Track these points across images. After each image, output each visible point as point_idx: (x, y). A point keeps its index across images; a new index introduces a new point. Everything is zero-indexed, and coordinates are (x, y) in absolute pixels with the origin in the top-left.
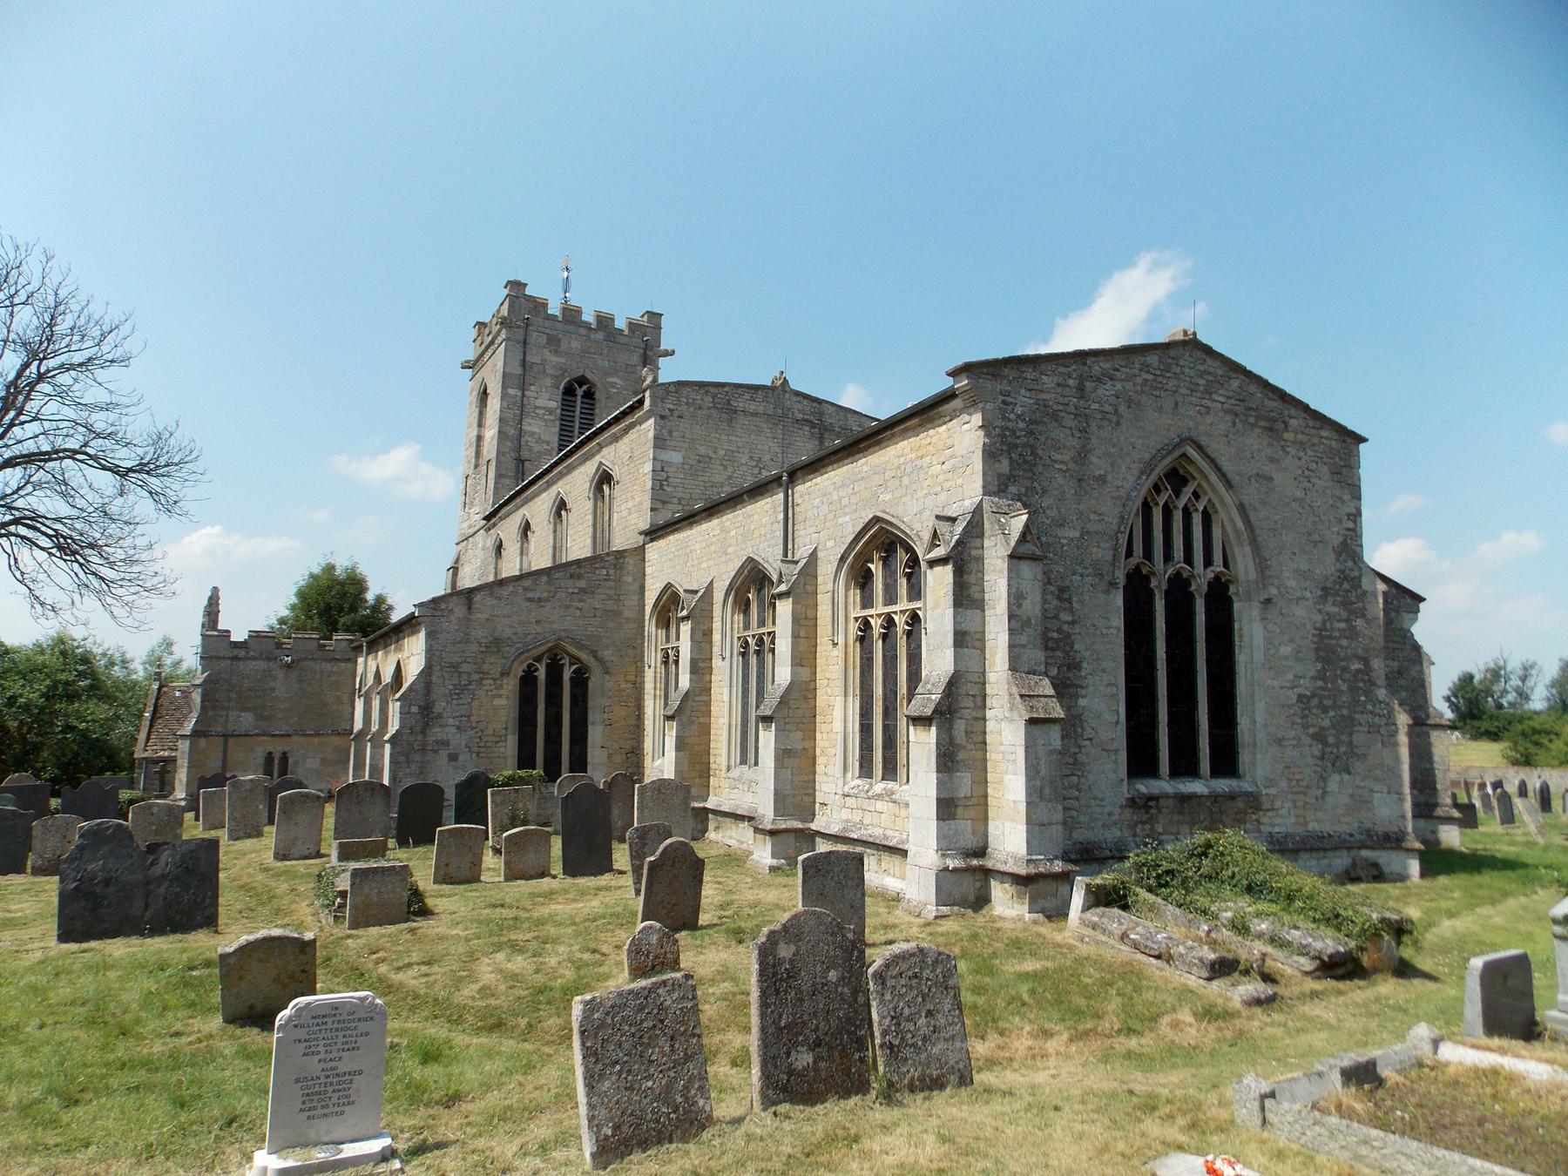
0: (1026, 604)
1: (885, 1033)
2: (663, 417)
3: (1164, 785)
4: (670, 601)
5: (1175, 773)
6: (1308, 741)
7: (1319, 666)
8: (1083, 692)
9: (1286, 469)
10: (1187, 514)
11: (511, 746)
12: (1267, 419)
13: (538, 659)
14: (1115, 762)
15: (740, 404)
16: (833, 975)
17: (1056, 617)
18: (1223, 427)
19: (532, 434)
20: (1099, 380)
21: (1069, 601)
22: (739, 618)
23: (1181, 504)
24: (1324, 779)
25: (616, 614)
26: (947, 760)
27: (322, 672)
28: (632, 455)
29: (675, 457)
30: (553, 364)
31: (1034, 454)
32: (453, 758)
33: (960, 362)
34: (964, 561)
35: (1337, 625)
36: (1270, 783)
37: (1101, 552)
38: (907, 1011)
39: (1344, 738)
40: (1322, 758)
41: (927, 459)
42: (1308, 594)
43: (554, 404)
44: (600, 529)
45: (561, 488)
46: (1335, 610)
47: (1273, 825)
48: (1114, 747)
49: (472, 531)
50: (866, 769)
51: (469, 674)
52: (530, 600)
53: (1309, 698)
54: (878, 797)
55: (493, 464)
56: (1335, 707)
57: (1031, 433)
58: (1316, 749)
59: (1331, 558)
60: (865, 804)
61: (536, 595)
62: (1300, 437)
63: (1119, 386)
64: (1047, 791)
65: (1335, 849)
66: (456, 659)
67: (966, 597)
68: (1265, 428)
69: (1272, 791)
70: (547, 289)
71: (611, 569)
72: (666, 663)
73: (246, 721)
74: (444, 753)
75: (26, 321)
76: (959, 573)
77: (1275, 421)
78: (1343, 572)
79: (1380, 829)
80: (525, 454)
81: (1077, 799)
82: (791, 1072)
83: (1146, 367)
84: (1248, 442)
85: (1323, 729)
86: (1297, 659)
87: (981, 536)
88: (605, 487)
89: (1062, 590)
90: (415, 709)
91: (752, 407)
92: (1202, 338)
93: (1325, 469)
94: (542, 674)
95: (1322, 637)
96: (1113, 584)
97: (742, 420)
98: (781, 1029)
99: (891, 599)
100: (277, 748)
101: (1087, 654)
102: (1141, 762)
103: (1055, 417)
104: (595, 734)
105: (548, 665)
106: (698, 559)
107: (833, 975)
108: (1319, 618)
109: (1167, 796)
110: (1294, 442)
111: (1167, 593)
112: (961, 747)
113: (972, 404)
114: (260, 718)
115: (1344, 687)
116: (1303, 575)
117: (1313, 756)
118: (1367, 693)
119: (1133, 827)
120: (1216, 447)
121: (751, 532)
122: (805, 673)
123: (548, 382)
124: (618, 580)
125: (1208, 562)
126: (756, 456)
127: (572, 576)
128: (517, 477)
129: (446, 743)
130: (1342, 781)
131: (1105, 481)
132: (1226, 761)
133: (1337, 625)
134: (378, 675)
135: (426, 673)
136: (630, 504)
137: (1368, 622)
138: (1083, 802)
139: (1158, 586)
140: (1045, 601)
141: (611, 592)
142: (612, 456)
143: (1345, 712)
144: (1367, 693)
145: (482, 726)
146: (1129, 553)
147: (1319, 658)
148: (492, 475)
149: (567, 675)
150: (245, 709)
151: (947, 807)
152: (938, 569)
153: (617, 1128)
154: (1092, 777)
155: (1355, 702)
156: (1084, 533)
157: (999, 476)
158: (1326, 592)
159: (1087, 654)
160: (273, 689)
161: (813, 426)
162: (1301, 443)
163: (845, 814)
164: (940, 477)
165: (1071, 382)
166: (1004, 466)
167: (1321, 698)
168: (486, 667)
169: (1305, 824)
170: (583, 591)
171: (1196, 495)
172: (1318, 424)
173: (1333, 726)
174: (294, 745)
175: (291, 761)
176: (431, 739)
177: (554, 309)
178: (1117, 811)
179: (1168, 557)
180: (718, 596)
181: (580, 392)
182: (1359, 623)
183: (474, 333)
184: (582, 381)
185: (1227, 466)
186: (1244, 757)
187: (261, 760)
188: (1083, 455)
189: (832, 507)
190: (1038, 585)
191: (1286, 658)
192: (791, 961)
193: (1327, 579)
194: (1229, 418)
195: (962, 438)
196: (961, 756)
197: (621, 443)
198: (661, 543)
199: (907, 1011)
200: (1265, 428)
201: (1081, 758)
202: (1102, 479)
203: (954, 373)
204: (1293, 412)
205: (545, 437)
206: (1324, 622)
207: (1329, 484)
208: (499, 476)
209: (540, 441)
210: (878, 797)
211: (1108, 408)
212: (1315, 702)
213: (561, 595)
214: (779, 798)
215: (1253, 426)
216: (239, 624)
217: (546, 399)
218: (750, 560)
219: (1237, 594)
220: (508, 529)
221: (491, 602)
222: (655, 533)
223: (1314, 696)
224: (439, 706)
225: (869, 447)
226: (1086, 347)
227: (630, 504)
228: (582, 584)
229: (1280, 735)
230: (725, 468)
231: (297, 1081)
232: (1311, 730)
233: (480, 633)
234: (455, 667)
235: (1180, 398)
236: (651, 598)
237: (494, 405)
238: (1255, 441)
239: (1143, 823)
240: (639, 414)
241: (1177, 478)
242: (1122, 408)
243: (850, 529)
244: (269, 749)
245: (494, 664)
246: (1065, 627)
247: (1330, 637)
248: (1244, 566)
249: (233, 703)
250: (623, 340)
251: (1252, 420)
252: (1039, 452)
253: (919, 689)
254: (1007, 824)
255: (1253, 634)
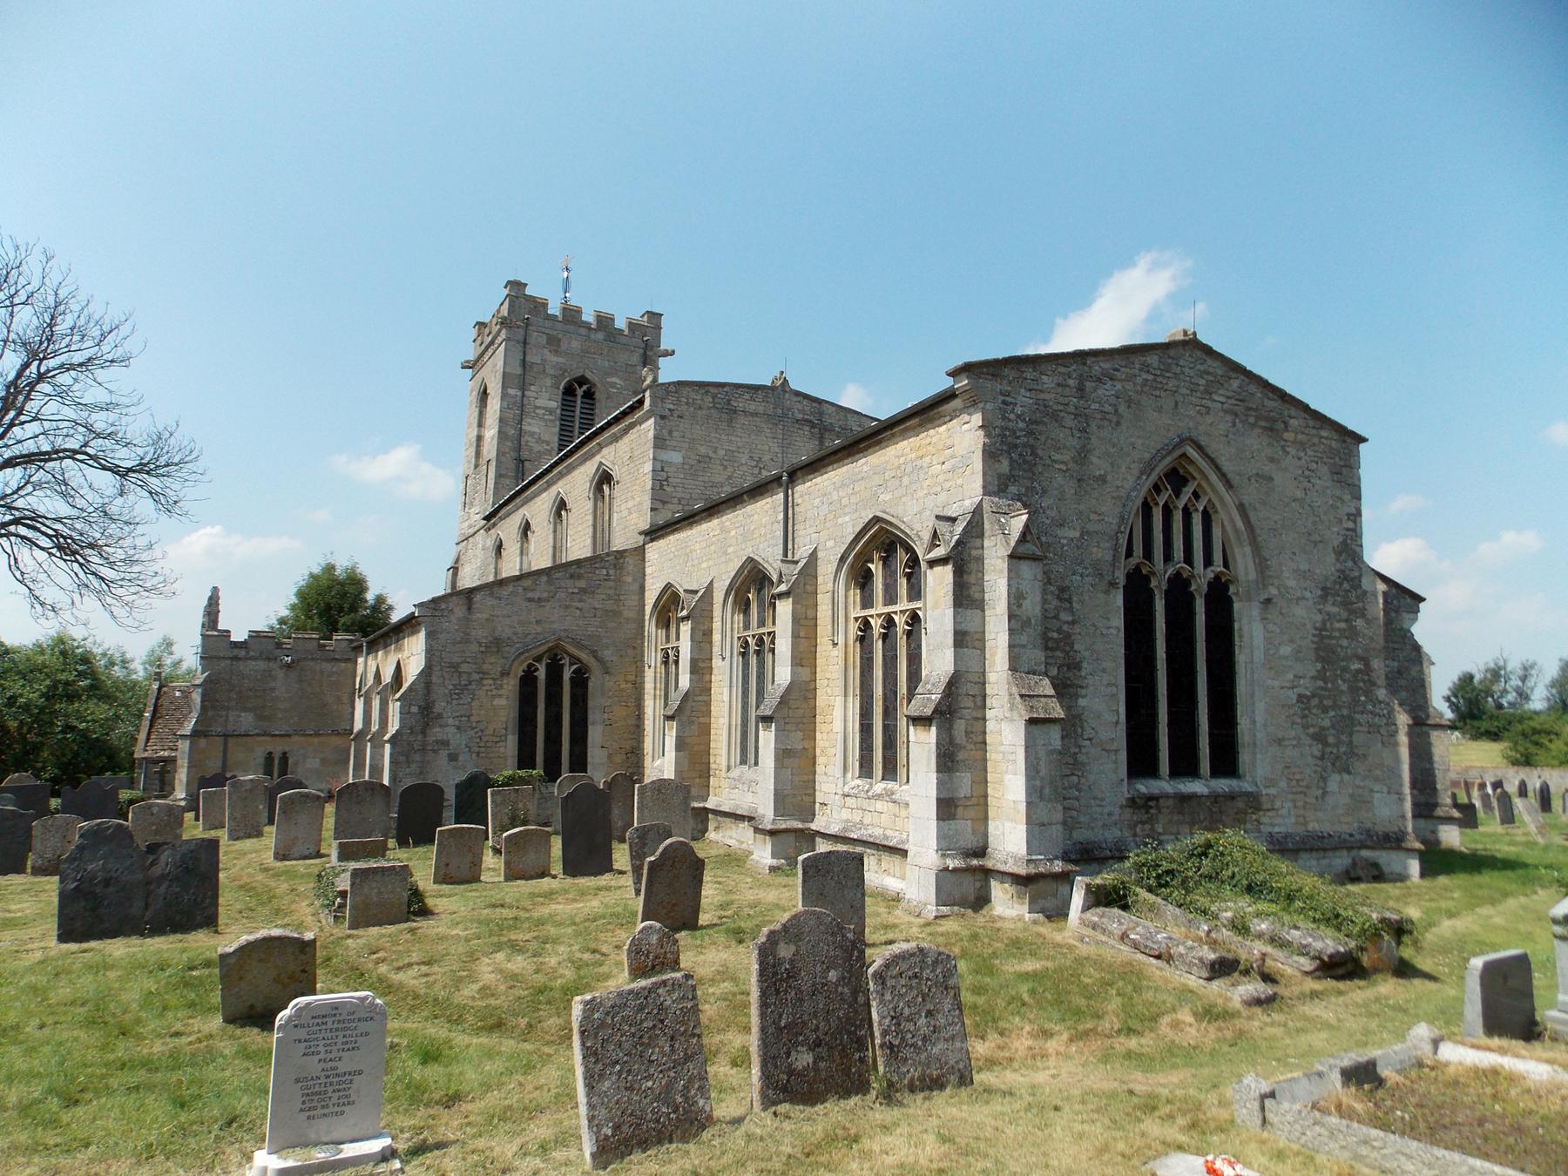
0: (1026, 604)
1: (885, 1033)
2: (663, 417)
3: (1164, 785)
4: (670, 601)
5: (1175, 773)
6: (1308, 741)
7: (1319, 666)
8: (1083, 692)
9: (1286, 469)
10: (1187, 514)
11: (511, 746)
12: (1267, 419)
13: (538, 659)
14: (1115, 762)
15: (740, 404)
16: (833, 975)
17: (1056, 617)
18: (1223, 427)
19: (532, 434)
20: (1099, 380)
21: (1069, 601)
22: (739, 618)
23: (1181, 504)
24: (1324, 779)
25: (616, 614)
26: (947, 760)
27: (322, 672)
28: (632, 455)
29: (675, 457)
30: (553, 364)
31: (1034, 454)
32: (453, 758)
33: (960, 362)
34: (964, 561)
35: (1337, 625)
36: (1270, 783)
37: (1101, 552)
38: (907, 1011)
39: (1344, 738)
40: (1322, 758)
41: (927, 459)
42: (1308, 594)
43: (554, 404)
44: (600, 529)
45: (561, 488)
46: (1335, 610)
47: (1273, 825)
48: (1114, 747)
49: (472, 531)
50: (866, 769)
51: (469, 674)
52: (530, 600)
53: (1309, 698)
54: (878, 797)
55: (493, 464)
56: (1335, 707)
57: (1031, 433)
58: (1316, 749)
59: (1331, 558)
60: (865, 804)
61: (536, 595)
62: (1300, 437)
63: (1119, 386)
64: (1047, 791)
65: (1335, 849)
66: (456, 659)
67: (966, 597)
68: (1265, 428)
69: (1272, 791)
70: (547, 289)
71: (611, 569)
72: (666, 663)
73: (246, 721)
74: (444, 753)
75: (26, 321)
76: (959, 573)
77: (1275, 421)
78: (1343, 572)
79: (1380, 829)
80: (525, 454)
81: (1077, 799)
82: (791, 1072)
83: (1146, 367)
84: (1248, 442)
85: (1323, 729)
86: (1297, 659)
87: (981, 536)
88: (605, 487)
89: (1062, 590)
90: (415, 709)
91: (752, 407)
92: (1202, 338)
93: (1325, 469)
94: (542, 674)
95: (1322, 637)
96: (1113, 584)
97: (742, 420)
98: (781, 1029)
99: (891, 599)
100: (277, 748)
101: (1087, 654)
102: (1141, 762)
103: (1055, 417)
104: (595, 734)
105: (548, 665)
106: (698, 559)
107: (833, 975)
108: (1319, 618)
109: (1167, 796)
110: (1294, 442)
111: (1167, 593)
112: (961, 747)
113: (972, 404)
114: (260, 718)
115: (1344, 687)
116: (1303, 575)
117: (1313, 756)
118: (1367, 693)
119: (1133, 827)
120: (1216, 447)
121: (751, 532)
122: (805, 673)
123: (548, 382)
124: (618, 580)
125: (1208, 562)
126: (756, 456)
127: (572, 576)
128: (517, 477)
129: (446, 743)
130: (1342, 781)
131: (1105, 481)
132: (1226, 761)
133: (1337, 625)
134: (378, 675)
135: (426, 673)
136: (630, 504)
137: (1368, 622)
138: (1083, 802)
139: (1158, 586)
140: (1045, 601)
141: (611, 592)
142: (612, 456)
143: (1345, 712)
144: (1367, 693)
145: (482, 726)
146: (1129, 553)
147: (1319, 658)
148: (492, 475)
149: (567, 675)
150: (245, 709)
151: (947, 807)
152: (938, 569)
153: (617, 1128)
154: (1092, 777)
155: (1355, 702)
156: (1084, 533)
157: (999, 476)
158: (1326, 592)
159: (1087, 654)
160: (273, 689)
161: (813, 426)
162: (1301, 443)
163: (845, 814)
164: (940, 477)
165: (1071, 382)
166: (1004, 466)
167: (1321, 698)
168: (486, 667)
169: (1305, 824)
170: (583, 591)
171: (1196, 495)
172: (1318, 424)
173: (1333, 726)
174: (294, 745)
175: (291, 761)
176: (431, 739)
177: (554, 309)
178: (1117, 811)
179: (1168, 557)
180: (718, 596)
181: (580, 392)
182: (1359, 623)
183: (474, 333)
184: (582, 381)
185: (1227, 466)
186: (1244, 757)
187: (261, 760)
188: (1083, 455)
189: (832, 507)
190: (1038, 585)
191: (1286, 658)
192: (791, 961)
193: (1327, 579)
194: (1229, 418)
195: (962, 438)
196: (961, 756)
197: (621, 443)
198: (661, 543)
199: (907, 1011)
200: (1265, 428)
201: (1081, 758)
202: (1102, 479)
203: (954, 373)
204: (1293, 412)
205: (545, 437)
206: (1324, 622)
207: (1329, 484)
208: (499, 476)
209: (540, 441)
210: (878, 797)
211: (1108, 408)
212: (1315, 702)
213: (561, 595)
214: (779, 798)
215: (1253, 426)
216: (239, 624)
217: (546, 399)
218: (750, 560)
219: (1237, 594)
220: (508, 529)
221: (491, 602)
222: (655, 533)
223: (1314, 696)
224: (439, 706)
225: (869, 447)
226: (1086, 347)
227: (630, 504)
228: (582, 584)
229: (1280, 735)
230: (725, 468)
231: (297, 1081)
232: (1311, 730)
233: (480, 633)
234: (455, 667)
235: (1180, 398)
236: (651, 598)
237: (494, 405)
238: (1255, 441)
239: (1143, 823)
240: (639, 414)
241: (1177, 478)
242: (1122, 408)
243: (850, 529)
244: (269, 749)
245: (494, 664)
246: (1065, 627)
247: (1330, 637)
248: (1244, 566)
249: (233, 703)
250: (623, 340)
251: (1252, 420)
252: (1039, 452)
253: (919, 689)
254: (1007, 824)
255: (1253, 634)
